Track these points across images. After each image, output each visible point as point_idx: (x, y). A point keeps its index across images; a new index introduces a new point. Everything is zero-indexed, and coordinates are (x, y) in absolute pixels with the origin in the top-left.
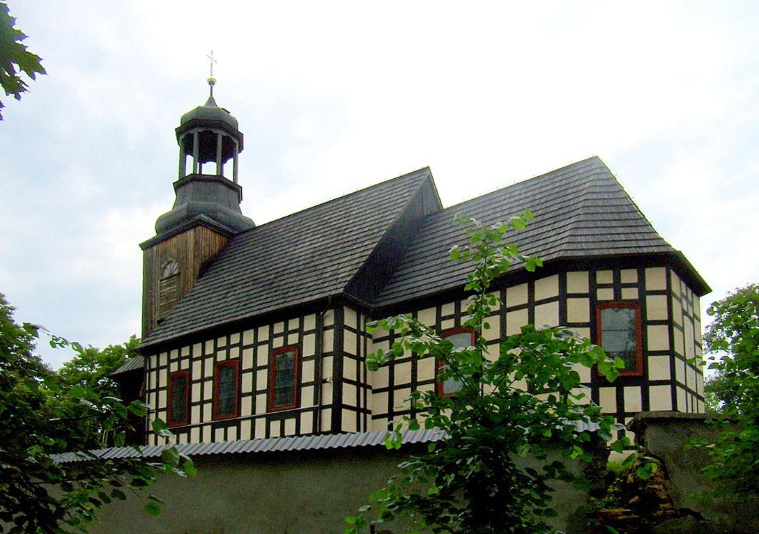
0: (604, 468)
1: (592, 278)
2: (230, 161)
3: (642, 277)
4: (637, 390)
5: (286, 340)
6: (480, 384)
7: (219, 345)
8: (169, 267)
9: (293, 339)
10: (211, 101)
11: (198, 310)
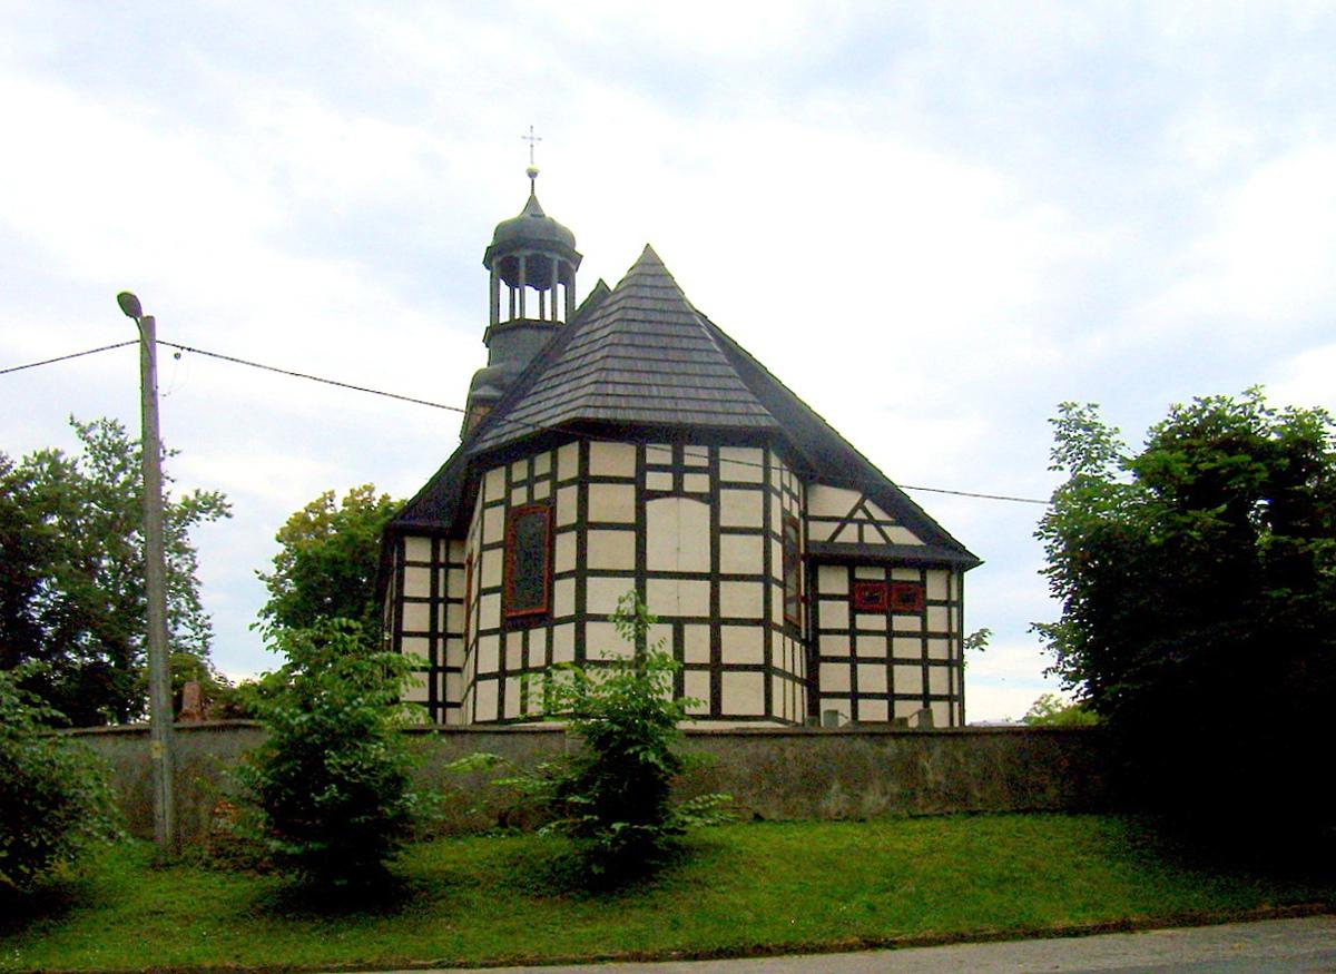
1: (641, 455)
2: (578, 302)
3: (714, 458)
5: (531, 494)
6: (804, 677)
9: (542, 490)
10: (532, 202)
11: (555, 406)
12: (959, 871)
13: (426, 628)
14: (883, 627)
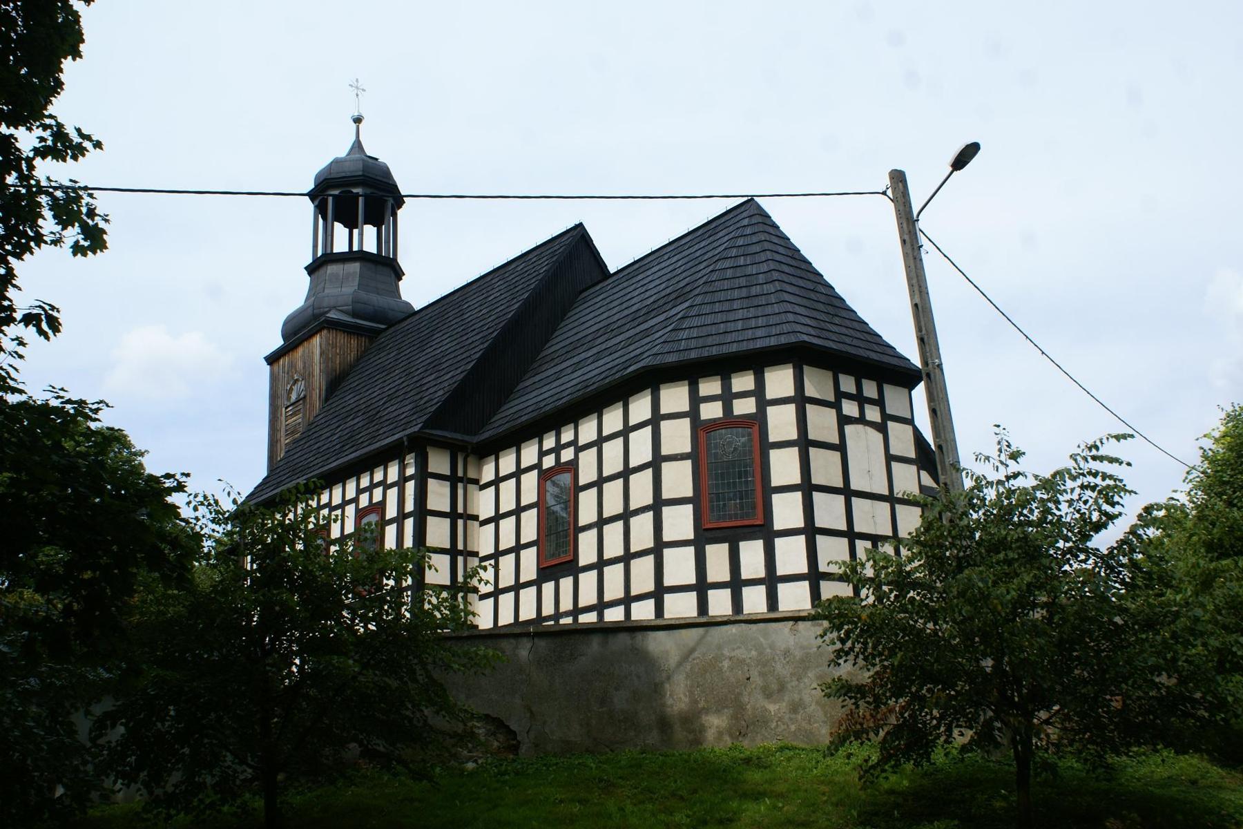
0: (146, 785)
4: (758, 545)
5: (558, 458)
7: (853, 390)
8: (295, 388)
9: (567, 455)
10: (358, 145)
12: (1093, 488)
13: (447, 545)
14: (745, 575)
